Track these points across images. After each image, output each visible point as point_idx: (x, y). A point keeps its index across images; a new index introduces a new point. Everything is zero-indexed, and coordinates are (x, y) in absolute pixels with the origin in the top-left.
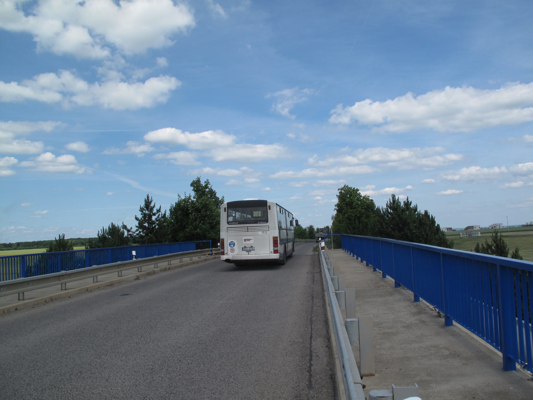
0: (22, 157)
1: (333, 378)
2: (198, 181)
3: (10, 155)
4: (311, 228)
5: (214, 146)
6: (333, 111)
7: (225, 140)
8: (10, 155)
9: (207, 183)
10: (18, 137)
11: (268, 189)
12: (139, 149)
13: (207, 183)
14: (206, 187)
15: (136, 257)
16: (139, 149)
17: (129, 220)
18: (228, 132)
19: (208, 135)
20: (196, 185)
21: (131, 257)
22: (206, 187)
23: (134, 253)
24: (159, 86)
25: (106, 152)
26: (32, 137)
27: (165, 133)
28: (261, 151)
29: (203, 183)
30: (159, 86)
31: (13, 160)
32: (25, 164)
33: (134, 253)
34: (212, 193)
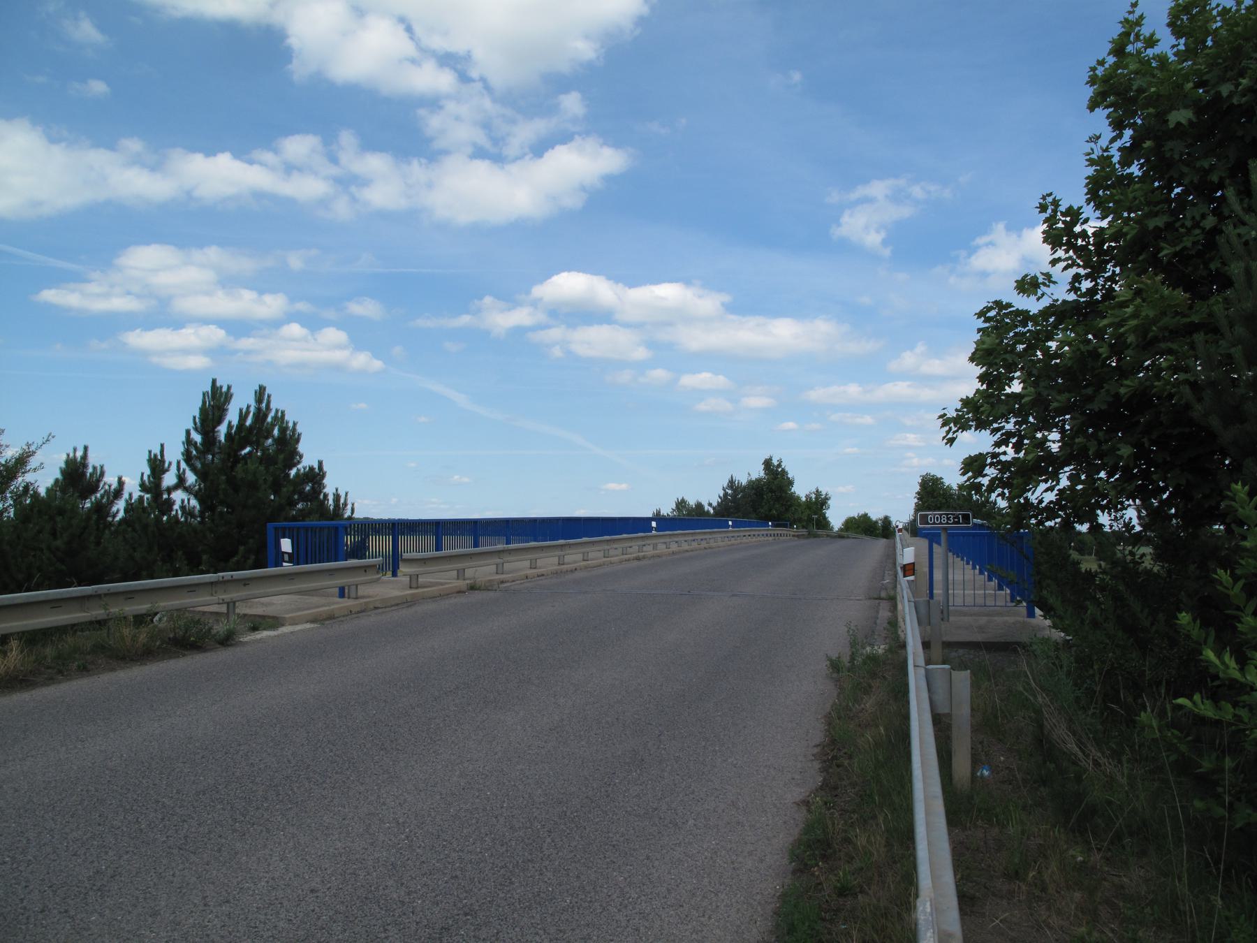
0: (238, 327)
1: (990, 646)
2: (771, 459)
3: (205, 321)
4: (886, 521)
5: (680, 317)
6: (981, 241)
7: (709, 304)
8: (205, 321)
9: (780, 462)
10: (229, 282)
11: (791, 425)
12: (503, 320)
13: (780, 462)
14: (779, 465)
15: (293, 558)
16: (503, 320)
17: (667, 509)
18: (710, 284)
19: (668, 293)
20: (768, 463)
21: (279, 558)
22: (779, 465)
23: (286, 545)
24: (579, 165)
25: (421, 323)
26: (261, 284)
27: (570, 284)
28: (783, 333)
29: (775, 463)
30: (579, 165)
31: (217, 335)
32: (247, 343)
33: (286, 545)
34: (784, 472)
